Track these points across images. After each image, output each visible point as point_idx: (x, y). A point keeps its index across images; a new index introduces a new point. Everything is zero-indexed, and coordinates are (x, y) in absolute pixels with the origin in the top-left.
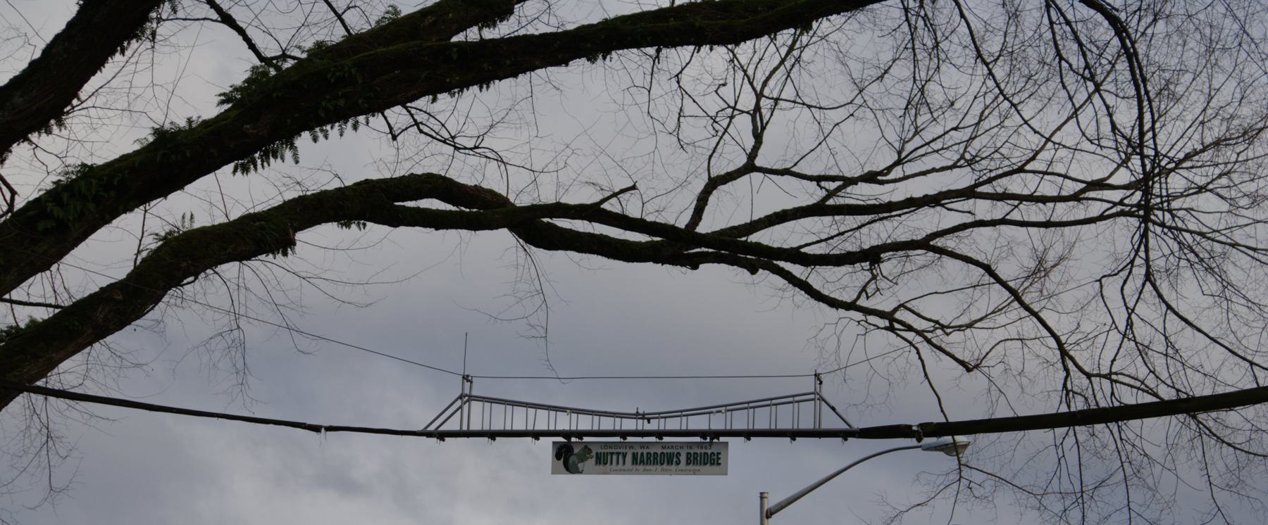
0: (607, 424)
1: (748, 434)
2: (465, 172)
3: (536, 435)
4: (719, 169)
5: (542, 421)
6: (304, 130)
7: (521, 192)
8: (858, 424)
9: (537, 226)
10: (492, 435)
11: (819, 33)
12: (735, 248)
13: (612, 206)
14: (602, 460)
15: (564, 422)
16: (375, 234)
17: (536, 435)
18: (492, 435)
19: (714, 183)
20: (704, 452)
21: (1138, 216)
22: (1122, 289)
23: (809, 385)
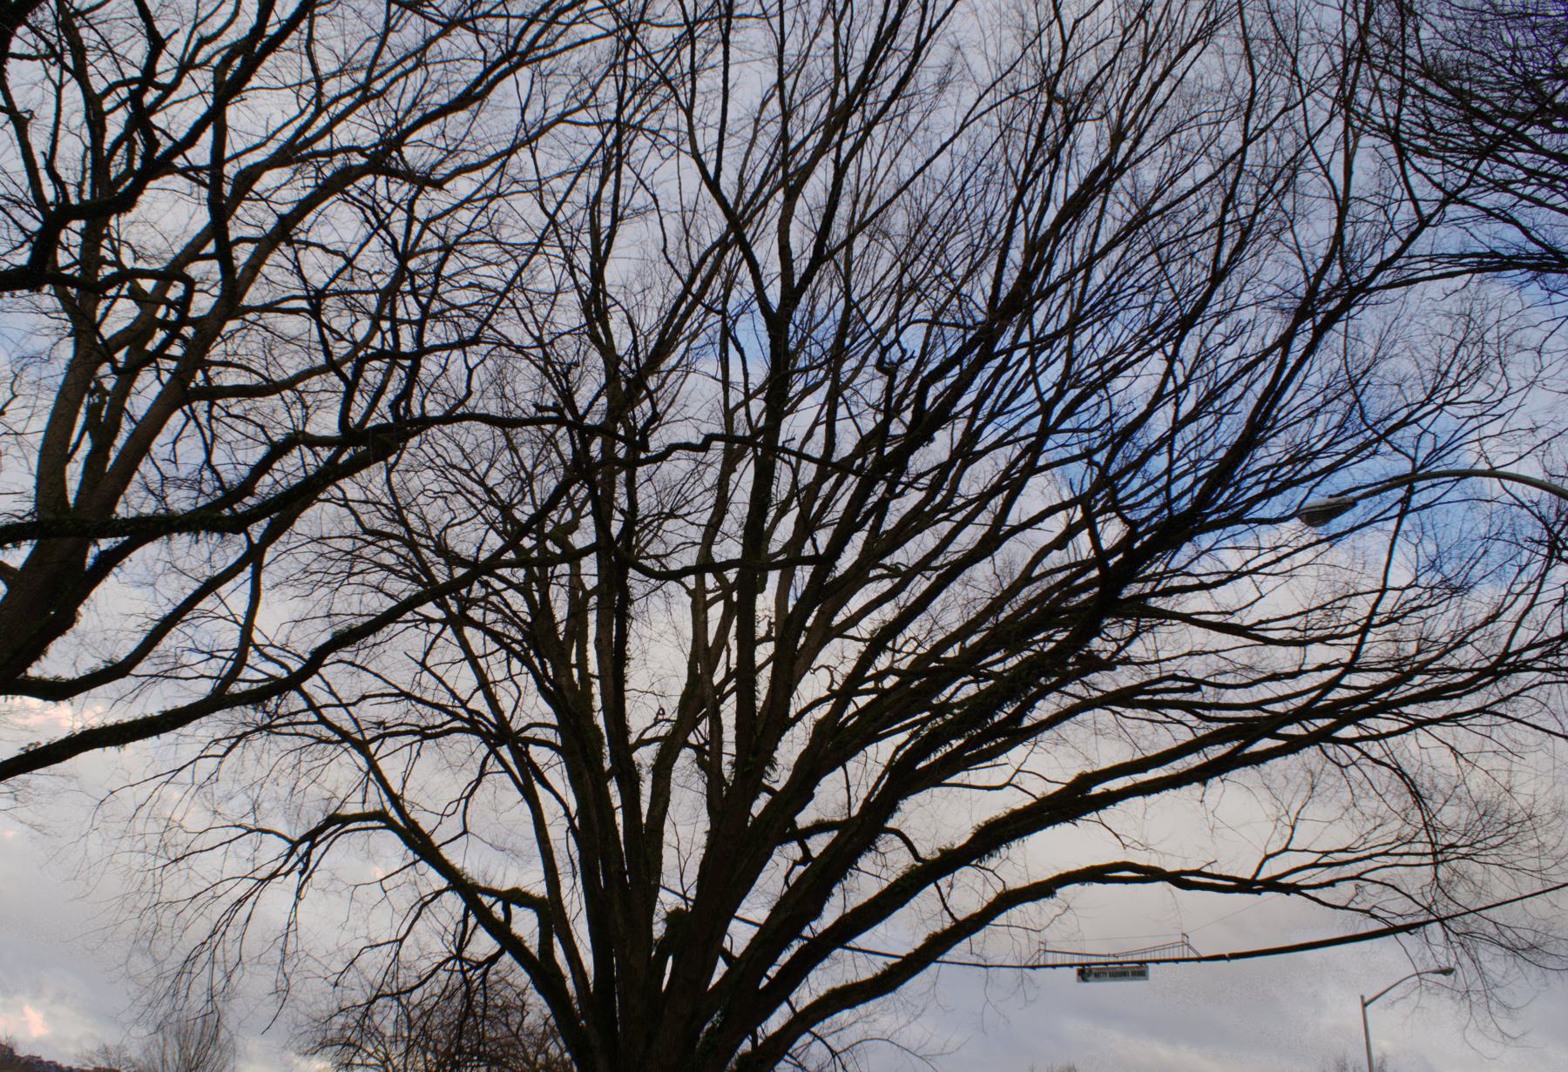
0: (1103, 960)
1: (1157, 962)
2: (1142, 859)
3: (1071, 966)
4: (1269, 852)
5: (1068, 959)
6: (290, 690)
7: (1171, 866)
8: (1204, 955)
9: (1179, 879)
10: (1054, 966)
11: (1177, 636)
12: (1272, 885)
13: (1207, 870)
14: (1097, 975)
15: (1085, 960)
16: (1097, 887)
17: (1071, 966)
18: (1054, 966)
19: (1267, 857)
20: (1136, 970)
21: (400, 153)
22: (1267, 857)
23: (1179, 938)
